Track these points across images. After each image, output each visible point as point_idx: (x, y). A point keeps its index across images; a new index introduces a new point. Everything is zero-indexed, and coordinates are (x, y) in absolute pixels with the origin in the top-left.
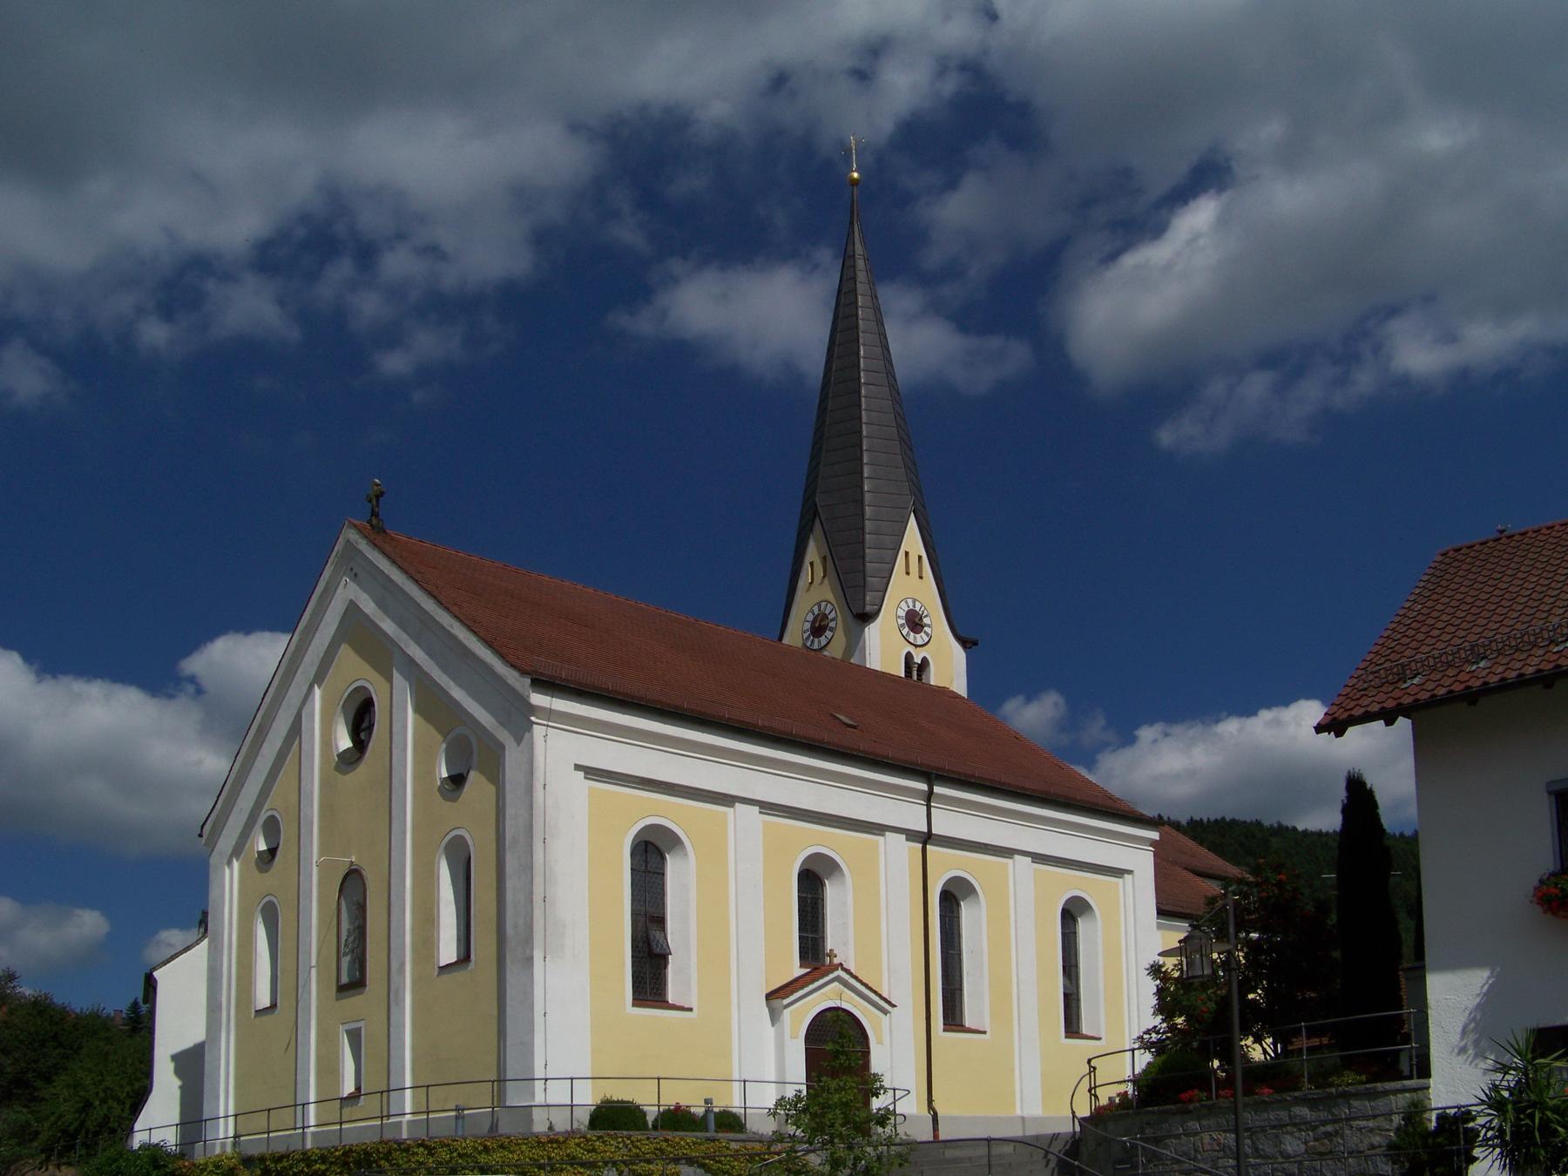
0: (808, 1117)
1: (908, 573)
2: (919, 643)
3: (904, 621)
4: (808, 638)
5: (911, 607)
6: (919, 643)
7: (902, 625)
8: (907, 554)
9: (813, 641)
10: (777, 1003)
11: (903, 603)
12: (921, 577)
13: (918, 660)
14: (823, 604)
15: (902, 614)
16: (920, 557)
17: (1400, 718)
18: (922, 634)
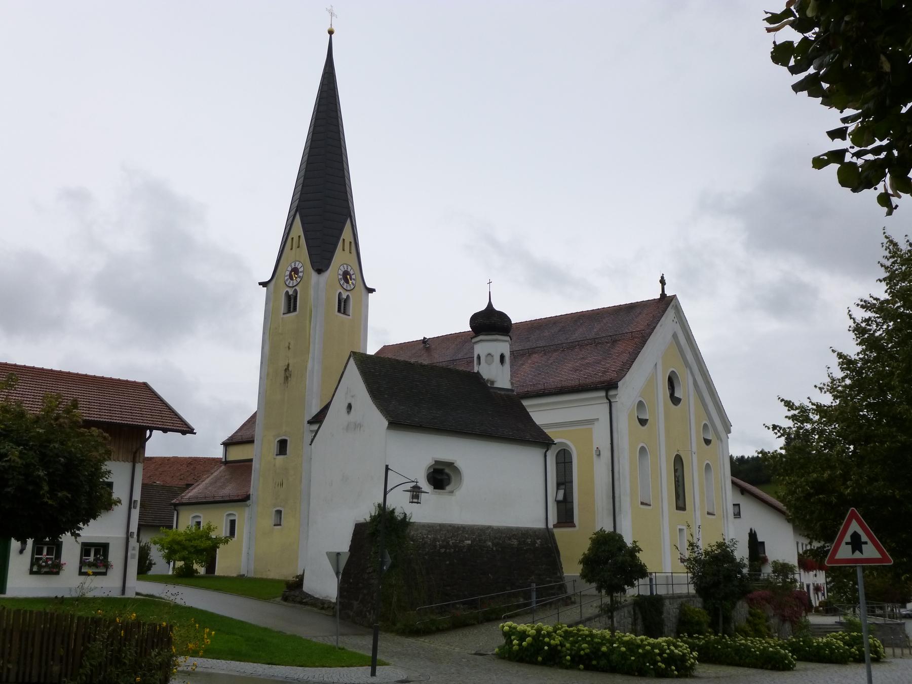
0: (157, 540)
1: (344, 250)
2: (349, 289)
3: (342, 277)
4: (287, 280)
5: (346, 269)
6: (348, 289)
7: (341, 279)
8: (344, 240)
9: (290, 282)
10: (246, 435)
11: (342, 267)
12: (351, 253)
13: (344, 296)
14: (297, 263)
15: (341, 272)
16: (350, 243)
17: (759, 541)
18: (296, 266)
